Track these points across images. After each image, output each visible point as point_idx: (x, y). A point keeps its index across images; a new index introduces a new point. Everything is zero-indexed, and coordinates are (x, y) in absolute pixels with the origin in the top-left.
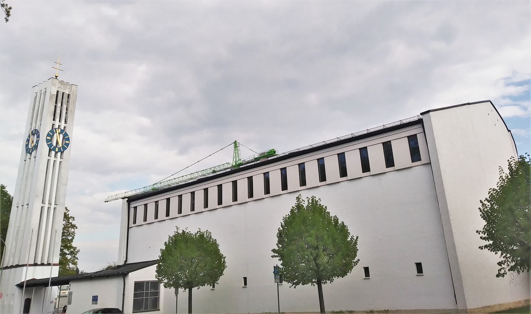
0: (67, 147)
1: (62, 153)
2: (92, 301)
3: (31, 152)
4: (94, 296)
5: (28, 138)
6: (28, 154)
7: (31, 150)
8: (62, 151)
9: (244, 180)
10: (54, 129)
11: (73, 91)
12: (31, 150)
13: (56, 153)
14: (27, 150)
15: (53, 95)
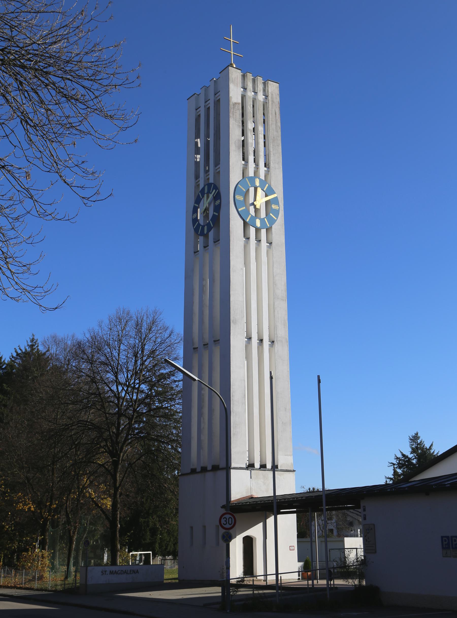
0: (276, 219)
1: (268, 230)
2: (443, 548)
3: (205, 232)
4: (448, 537)
5: (195, 205)
6: (201, 239)
7: (206, 228)
8: (269, 226)
9: (234, 434)
10: (247, 179)
11: (272, 95)
12: (206, 228)
13: (258, 230)
14: (196, 230)
15: (236, 103)
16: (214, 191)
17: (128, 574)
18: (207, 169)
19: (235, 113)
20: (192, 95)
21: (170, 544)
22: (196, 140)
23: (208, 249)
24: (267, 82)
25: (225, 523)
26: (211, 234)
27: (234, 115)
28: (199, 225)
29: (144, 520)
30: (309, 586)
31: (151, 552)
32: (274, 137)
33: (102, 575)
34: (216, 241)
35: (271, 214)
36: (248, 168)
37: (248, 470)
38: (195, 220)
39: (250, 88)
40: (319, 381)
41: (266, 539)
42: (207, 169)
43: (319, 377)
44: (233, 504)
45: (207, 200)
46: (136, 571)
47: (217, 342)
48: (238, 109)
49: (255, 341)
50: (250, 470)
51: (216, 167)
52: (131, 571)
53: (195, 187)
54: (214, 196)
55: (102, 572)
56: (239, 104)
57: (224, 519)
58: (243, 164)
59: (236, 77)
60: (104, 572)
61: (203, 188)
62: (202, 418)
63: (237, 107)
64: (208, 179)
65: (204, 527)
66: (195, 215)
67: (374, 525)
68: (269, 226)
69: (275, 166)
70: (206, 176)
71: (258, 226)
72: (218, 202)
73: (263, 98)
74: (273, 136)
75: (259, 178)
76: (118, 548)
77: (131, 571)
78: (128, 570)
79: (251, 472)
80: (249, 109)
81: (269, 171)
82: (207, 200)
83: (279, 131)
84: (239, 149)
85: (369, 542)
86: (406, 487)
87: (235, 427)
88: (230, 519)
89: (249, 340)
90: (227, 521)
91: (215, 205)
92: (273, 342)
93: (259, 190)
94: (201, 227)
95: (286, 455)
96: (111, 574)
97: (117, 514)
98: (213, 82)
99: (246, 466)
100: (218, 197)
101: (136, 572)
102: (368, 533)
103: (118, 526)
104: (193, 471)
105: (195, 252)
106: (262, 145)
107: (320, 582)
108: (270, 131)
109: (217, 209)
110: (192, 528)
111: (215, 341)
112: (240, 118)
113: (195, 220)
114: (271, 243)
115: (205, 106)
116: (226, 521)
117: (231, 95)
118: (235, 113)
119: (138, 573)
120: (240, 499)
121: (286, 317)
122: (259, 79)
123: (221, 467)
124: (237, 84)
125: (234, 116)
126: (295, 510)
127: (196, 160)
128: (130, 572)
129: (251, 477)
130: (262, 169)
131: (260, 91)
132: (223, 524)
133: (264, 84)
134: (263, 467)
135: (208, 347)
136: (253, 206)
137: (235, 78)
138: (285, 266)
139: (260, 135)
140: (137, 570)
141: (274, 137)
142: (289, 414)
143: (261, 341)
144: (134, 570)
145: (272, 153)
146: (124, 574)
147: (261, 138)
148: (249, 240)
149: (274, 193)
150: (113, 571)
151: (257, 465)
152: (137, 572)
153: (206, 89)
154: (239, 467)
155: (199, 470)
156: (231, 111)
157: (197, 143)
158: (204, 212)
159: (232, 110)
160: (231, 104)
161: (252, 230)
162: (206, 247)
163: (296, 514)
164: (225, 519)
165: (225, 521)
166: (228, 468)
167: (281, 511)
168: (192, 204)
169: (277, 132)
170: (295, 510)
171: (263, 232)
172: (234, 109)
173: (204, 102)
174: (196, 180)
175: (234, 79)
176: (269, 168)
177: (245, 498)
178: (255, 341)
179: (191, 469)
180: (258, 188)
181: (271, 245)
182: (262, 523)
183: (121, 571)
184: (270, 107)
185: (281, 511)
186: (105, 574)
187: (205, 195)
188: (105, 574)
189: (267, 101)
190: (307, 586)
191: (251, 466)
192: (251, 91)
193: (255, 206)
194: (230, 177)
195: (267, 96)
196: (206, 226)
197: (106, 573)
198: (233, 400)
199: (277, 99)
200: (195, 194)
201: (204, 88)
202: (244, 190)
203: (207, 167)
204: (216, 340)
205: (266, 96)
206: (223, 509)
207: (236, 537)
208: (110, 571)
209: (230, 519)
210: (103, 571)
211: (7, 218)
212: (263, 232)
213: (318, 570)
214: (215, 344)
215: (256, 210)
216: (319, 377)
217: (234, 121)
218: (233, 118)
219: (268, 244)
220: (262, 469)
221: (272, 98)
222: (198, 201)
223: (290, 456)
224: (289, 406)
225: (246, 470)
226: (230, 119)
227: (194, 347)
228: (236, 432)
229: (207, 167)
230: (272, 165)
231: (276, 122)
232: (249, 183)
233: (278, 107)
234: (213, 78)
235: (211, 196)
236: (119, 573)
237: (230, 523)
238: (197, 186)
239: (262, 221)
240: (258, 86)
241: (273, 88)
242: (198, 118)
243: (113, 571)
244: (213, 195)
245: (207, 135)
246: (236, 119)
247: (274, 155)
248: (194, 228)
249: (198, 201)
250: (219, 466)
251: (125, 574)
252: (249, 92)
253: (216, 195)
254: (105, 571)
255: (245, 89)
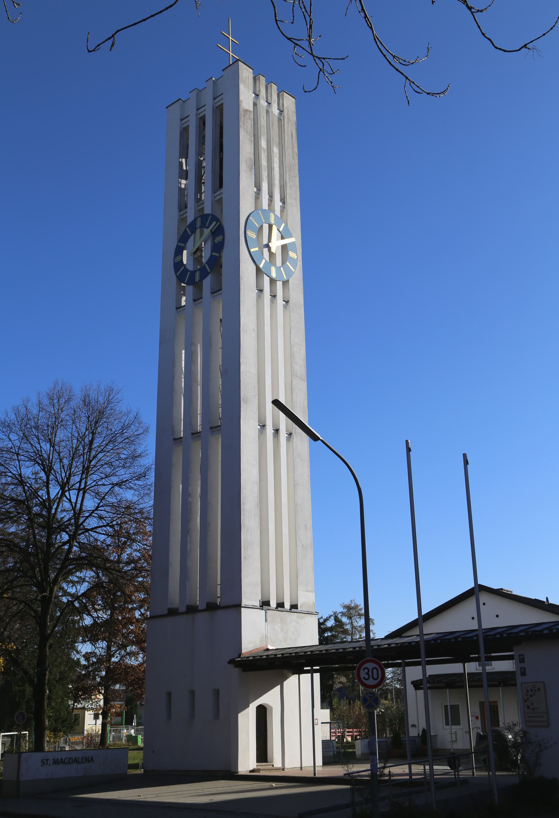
1: (285, 283)
7: (197, 274)
8: (285, 278)
9: (245, 558)
12: (197, 274)
13: (273, 281)
14: (181, 279)
16: (214, 223)
17: (79, 763)
18: (199, 197)
19: (246, 123)
20: (176, 100)
21: (51, 720)
22: (181, 160)
23: (202, 302)
24: (282, 93)
25: (367, 677)
26: (207, 283)
27: (245, 125)
28: (186, 270)
29: (19, 688)
30: (413, 777)
31: (27, 732)
32: (290, 165)
33: (42, 765)
34: (216, 290)
35: (288, 263)
36: (260, 198)
37: (262, 609)
38: (178, 265)
39: (263, 96)
40: (466, 462)
41: (314, 708)
42: (199, 197)
43: (465, 455)
44: (245, 657)
45: (200, 238)
46: (90, 758)
47: (215, 429)
48: (249, 119)
49: (270, 430)
50: (265, 610)
51: (214, 193)
52: (83, 759)
53: (178, 222)
54: (213, 231)
55: (42, 761)
56: (250, 111)
57: (364, 669)
58: (255, 192)
59: (247, 77)
60: (45, 761)
61: (194, 222)
62: (189, 536)
63: (248, 116)
64: (203, 209)
65: (192, 693)
66: (178, 259)
67: (544, 683)
68: (285, 278)
69: (292, 202)
70: (198, 206)
71: (274, 277)
72: (218, 239)
73: (278, 113)
74: (289, 164)
75: (274, 213)
76: (45, 725)
77: (83, 759)
78: (79, 758)
79: (266, 612)
80: (263, 121)
81: (284, 208)
82: (200, 238)
83: (296, 159)
84: (251, 170)
85: (533, 709)
86: (452, 638)
87: (246, 548)
88: (375, 671)
89: (262, 429)
90: (370, 673)
91: (214, 242)
92: (291, 434)
93: (274, 228)
94: (189, 273)
95: (307, 591)
96: (56, 764)
97: (45, 675)
98: (210, 82)
99: (260, 604)
100: (219, 231)
101: (91, 760)
102: (531, 696)
103: (46, 692)
104: (173, 612)
105: (177, 308)
106: (277, 171)
107: (476, 773)
108: (286, 156)
109: (218, 247)
110: (169, 694)
111: (211, 428)
112: (252, 131)
113: (178, 265)
114: (288, 302)
115: (196, 114)
116: (367, 673)
117: (241, 98)
118: (246, 123)
119: (93, 762)
120: (254, 652)
121: (306, 403)
122: (274, 86)
123: (180, 611)
124: (248, 86)
125: (245, 127)
126: (318, 668)
127: (180, 186)
128: (82, 760)
129: (266, 620)
130: (278, 204)
131: (274, 102)
132: (364, 678)
133: (278, 95)
134: (280, 605)
135: (200, 436)
136: (267, 249)
137: (246, 77)
138: (303, 334)
139: (275, 158)
140: (92, 758)
141: (290, 165)
142: (310, 535)
143: (277, 431)
144: (88, 758)
145: (288, 185)
146: (73, 763)
147: (276, 163)
148: (262, 293)
149: (291, 236)
150: (58, 759)
151: (273, 604)
152: (92, 760)
153: (199, 92)
154: (252, 606)
155: (183, 609)
156: (241, 119)
157: (181, 164)
158: (195, 253)
159: (242, 118)
160: (242, 109)
161: (266, 280)
162: (197, 298)
163: (319, 674)
164: (366, 671)
165: (366, 673)
166: (238, 606)
167: (471, 656)
168: (174, 243)
169: (294, 159)
170: (318, 668)
171: (279, 285)
172: (244, 117)
173: (195, 109)
174: (180, 212)
175: (244, 78)
176: (285, 204)
177: (259, 650)
178: (270, 430)
179: (169, 609)
180: (273, 226)
181: (287, 305)
182: (279, 685)
183: (70, 758)
184: (286, 124)
185: (471, 656)
186: (47, 764)
187: (198, 231)
188: (47, 764)
189: (282, 118)
190: (408, 777)
191: (265, 604)
192: (264, 99)
193: (270, 250)
194: (240, 205)
195: (282, 111)
196: (197, 272)
197: (49, 763)
198: (243, 509)
199: (294, 118)
200: (178, 230)
201: (195, 91)
202: (257, 226)
203: (199, 195)
204: (213, 426)
205: (281, 112)
206: (231, 665)
207: (249, 706)
208: (54, 760)
209: (375, 671)
210: (44, 759)
211: (109, 38)
212: (279, 285)
213: (473, 753)
214: (212, 432)
215: (271, 254)
216: (465, 455)
217: (245, 134)
218: (244, 128)
219: (284, 303)
220: (279, 609)
221: (288, 114)
222: (183, 239)
223: (312, 592)
224: (310, 524)
225: (260, 609)
226: (240, 128)
227: (174, 437)
228: (247, 555)
229: (199, 195)
230: (288, 200)
231: (293, 147)
232: (262, 218)
233: (295, 127)
234: (212, 78)
235: (207, 232)
236: (66, 762)
237: (375, 677)
238: (182, 220)
239: (278, 270)
240: (273, 95)
241: (289, 102)
242: (185, 131)
243: (58, 759)
244: (211, 231)
245: (200, 152)
246: (247, 131)
247: (290, 187)
248: (178, 274)
249: (183, 239)
250: (178, 609)
251: (75, 763)
252: (262, 101)
253: (215, 230)
254: (47, 760)
255: (257, 95)
